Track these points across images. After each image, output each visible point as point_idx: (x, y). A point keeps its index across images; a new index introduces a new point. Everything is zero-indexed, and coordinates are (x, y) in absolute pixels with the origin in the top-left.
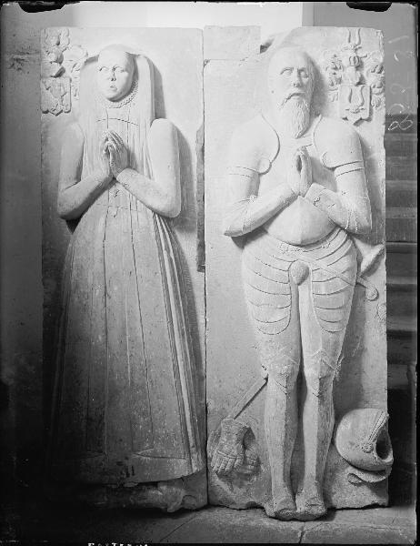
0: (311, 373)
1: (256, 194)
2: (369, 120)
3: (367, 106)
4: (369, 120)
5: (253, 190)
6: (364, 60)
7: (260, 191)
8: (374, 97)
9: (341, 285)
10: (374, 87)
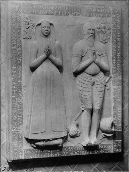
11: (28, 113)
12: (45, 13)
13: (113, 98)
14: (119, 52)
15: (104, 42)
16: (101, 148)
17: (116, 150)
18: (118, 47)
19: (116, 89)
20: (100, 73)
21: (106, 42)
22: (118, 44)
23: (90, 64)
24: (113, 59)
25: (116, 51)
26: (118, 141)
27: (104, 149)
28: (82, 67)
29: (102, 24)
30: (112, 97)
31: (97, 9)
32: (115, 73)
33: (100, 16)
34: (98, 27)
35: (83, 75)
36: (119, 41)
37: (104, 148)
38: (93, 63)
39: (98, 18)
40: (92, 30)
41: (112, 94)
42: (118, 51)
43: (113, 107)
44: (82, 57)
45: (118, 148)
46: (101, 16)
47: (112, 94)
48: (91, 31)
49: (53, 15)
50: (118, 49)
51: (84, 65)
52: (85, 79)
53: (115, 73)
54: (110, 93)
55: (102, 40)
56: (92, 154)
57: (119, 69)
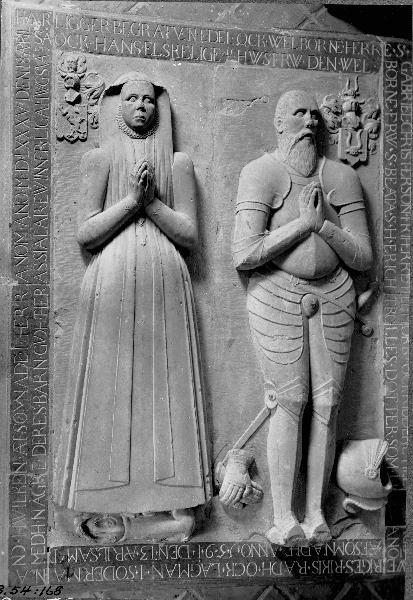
1: (269, 229)
2: (366, 163)
3: (365, 150)
5: (268, 226)
17: (397, 563)
27: (352, 558)
33: (339, 68)
37: (353, 553)
38: (313, 234)
51: (279, 241)
52: (282, 293)
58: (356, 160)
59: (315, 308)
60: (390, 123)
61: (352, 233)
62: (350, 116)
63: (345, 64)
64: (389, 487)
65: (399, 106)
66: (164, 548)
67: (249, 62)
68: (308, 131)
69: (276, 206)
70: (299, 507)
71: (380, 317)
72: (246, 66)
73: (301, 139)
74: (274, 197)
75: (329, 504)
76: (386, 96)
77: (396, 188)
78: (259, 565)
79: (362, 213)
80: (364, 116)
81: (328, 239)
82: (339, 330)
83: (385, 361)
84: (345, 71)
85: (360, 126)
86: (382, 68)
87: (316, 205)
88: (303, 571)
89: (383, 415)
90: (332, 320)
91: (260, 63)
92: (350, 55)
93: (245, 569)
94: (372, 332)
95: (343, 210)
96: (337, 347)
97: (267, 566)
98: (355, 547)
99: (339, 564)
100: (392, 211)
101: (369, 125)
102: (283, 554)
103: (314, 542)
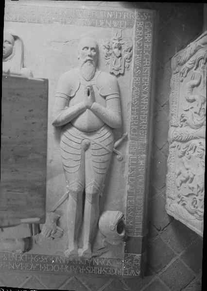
0: (89, 191)
1: (68, 106)
2: (123, 74)
3: (123, 68)
4: (198, 85)
5: (67, 104)
6: (122, 46)
7: (70, 105)
8: (126, 63)
9: (104, 152)
10: (127, 59)
11: (18, 192)
12: (11, 19)
13: (129, 176)
14: (145, 93)
15: (116, 73)
16: (100, 264)
17: (130, 272)
18: (144, 83)
19: (137, 160)
20: (102, 129)
21: (120, 74)
22: (146, 78)
23: (80, 112)
24: (133, 105)
25: (141, 90)
26: (135, 256)
27: (106, 266)
28: (66, 115)
29: (115, 40)
30: (127, 173)
31: (108, 14)
32: (134, 131)
33: (112, 26)
34: (107, 46)
35: (72, 132)
36: (147, 73)
37: (107, 265)
38: (87, 110)
39: (108, 29)
40: (89, 49)
41: (127, 169)
42: (144, 90)
43: (128, 192)
44: (71, 98)
45: (134, 269)
46: (115, 25)
47: (127, 169)
48: (88, 52)
49: (25, 22)
50: (145, 86)
51: (70, 113)
52: (73, 138)
53: (134, 131)
54: (124, 166)
55: (114, 69)
56: (141, 272)
57: (143, 124)
58: (118, 73)
59: (87, 147)
60: (138, 54)
61: (110, 111)
62: (116, 50)
63: (115, 24)
64: (123, 234)
65: (143, 45)
66: (15, 255)
67: (65, 23)
68: (89, 58)
69: (72, 96)
70: (78, 238)
71: (127, 152)
72: (63, 25)
73: (86, 62)
74: (71, 91)
75: (93, 241)
76: (136, 40)
77: (140, 87)
78: (60, 267)
79: (119, 99)
80: (123, 50)
81: (96, 112)
82: (100, 157)
83: (129, 173)
84: (115, 28)
85: (120, 56)
86: (135, 25)
87: (89, 95)
88: (82, 271)
89: (126, 199)
90: (64, 146)
91: (71, 24)
92: (117, 20)
93: (53, 268)
94: (123, 158)
95: (107, 98)
96: (98, 165)
97: (64, 267)
98: (108, 261)
99: (100, 269)
100: (137, 99)
101: (126, 55)
102: (72, 263)
103: (82, 258)
